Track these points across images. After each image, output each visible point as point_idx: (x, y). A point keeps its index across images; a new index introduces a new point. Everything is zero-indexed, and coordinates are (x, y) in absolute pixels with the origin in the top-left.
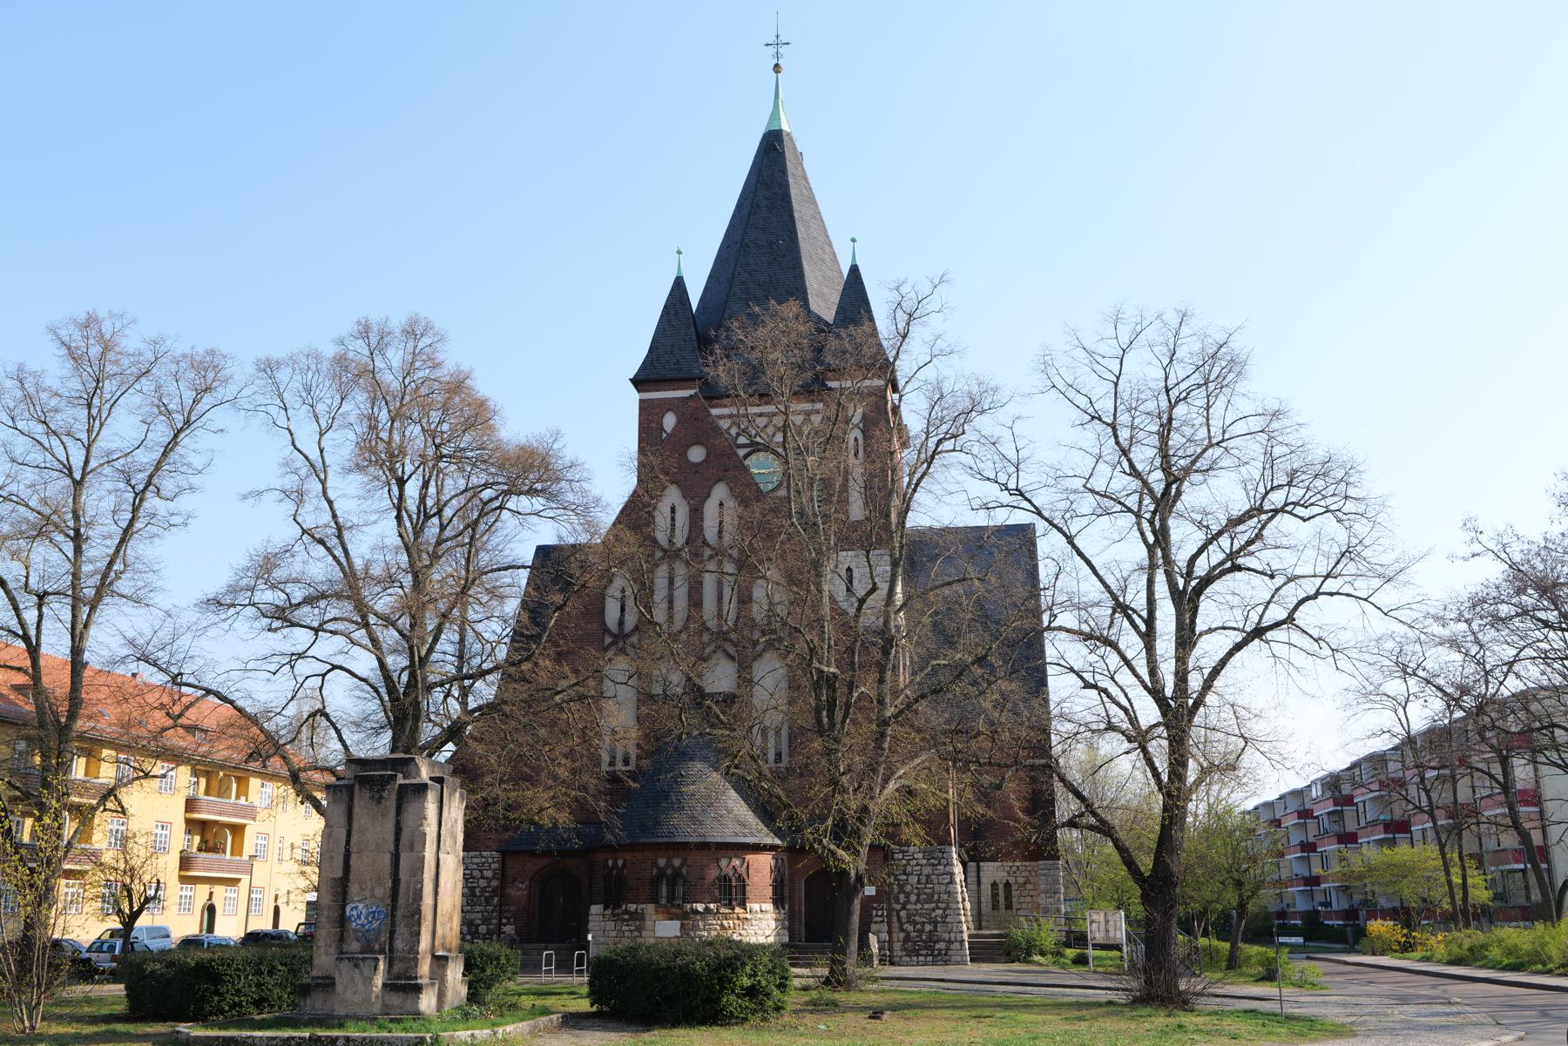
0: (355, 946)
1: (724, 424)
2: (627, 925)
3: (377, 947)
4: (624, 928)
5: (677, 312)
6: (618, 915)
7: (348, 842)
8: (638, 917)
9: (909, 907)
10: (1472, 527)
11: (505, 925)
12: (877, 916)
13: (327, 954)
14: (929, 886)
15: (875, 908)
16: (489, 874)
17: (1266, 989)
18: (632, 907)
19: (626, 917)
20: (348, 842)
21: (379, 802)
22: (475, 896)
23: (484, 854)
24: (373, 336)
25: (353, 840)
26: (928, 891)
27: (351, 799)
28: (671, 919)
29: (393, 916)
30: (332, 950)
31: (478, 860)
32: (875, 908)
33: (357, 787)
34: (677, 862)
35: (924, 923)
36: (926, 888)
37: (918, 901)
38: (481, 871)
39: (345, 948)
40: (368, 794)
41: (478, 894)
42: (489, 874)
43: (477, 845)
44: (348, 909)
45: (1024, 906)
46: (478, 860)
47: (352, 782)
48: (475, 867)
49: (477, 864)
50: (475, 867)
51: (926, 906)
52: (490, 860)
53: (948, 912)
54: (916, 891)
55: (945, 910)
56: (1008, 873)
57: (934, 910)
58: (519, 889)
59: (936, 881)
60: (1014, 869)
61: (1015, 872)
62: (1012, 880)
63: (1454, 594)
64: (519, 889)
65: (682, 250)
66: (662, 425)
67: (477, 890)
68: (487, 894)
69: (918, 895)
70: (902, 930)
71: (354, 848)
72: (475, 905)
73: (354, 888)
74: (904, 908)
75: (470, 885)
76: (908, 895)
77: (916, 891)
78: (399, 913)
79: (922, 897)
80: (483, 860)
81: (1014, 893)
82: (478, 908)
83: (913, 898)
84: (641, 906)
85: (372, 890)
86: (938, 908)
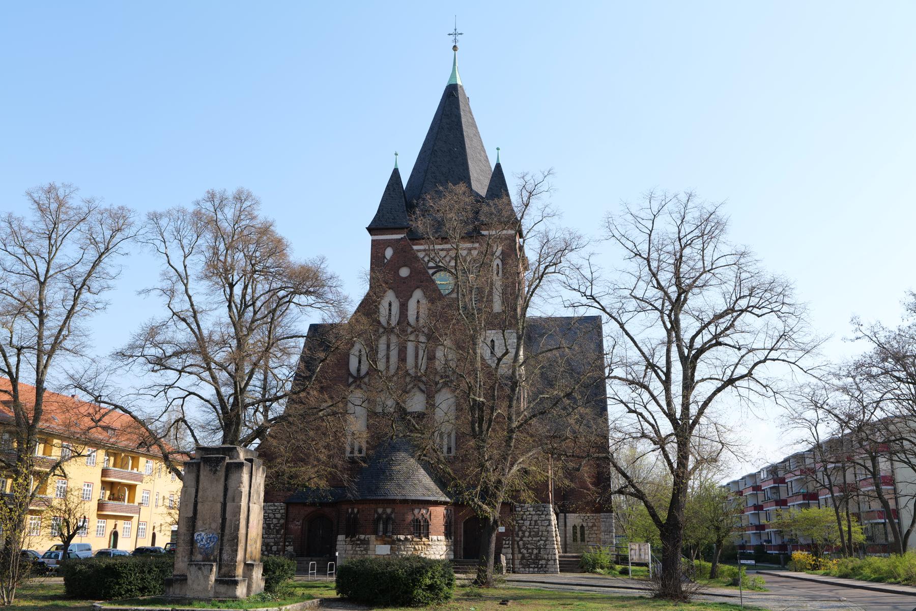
0: (199, 557)
1: (421, 255)
2: (359, 547)
3: (212, 558)
4: (357, 549)
6: (354, 541)
7: (196, 496)
8: (366, 542)
9: (524, 539)
11: (287, 546)
12: (505, 544)
15: (504, 540)
16: (278, 516)
18: (362, 537)
19: (359, 542)
20: (196, 496)
23: (276, 504)
25: (200, 494)
26: (535, 530)
27: (199, 471)
28: (385, 544)
29: (222, 540)
31: (272, 508)
32: (504, 540)
33: (202, 464)
34: (389, 511)
35: (533, 549)
36: (534, 528)
37: (530, 536)
38: (274, 514)
39: (193, 558)
41: (272, 528)
42: (278, 516)
43: (272, 499)
45: (592, 539)
46: (272, 508)
47: (199, 461)
48: (271, 511)
49: (272, 510)
50: (271, 511)
51: (534, 539)
52: (280, 508)
53: (547, 542)
54: (528, 530)
55: (545, 541)
57: (539, 541)
59: (540, 524)
60: (586, 518)
62: (585, 524)
67: (272, 525)
69: (530, 532)
71: (199, 500)
73: (199, 523)
74: (521, 540)
75: (267, 522)
76: (524, 532)
77: (528, 530)
78: (226, 538)
80: (276, 508)
82: (272, 536)
83: (527, 534)
84: (367, 536)
86: (542, 540)
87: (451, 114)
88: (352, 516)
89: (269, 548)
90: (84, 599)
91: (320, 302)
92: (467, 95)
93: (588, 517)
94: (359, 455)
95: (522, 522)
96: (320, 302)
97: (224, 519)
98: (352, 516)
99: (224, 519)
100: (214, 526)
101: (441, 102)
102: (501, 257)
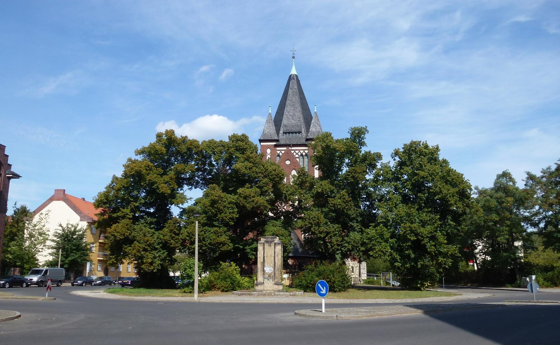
0: (267, 276)
1: (292, 152)
3: (272, 276)
5: (270, 122)
7: (264, 255)
10: (181, 136)
13: (261, 277)
20: (264, 255)
21: (270, 246)
24: (378, 153)
25: (265, 253)
27: (264, 246)
29: (275, 270)
30: (262, 277)
33: (265, 243)
39: (265, 276)
40: (268, 245)
44: (265, 268)
45: (357, 272)
47: (264, 242)
62: (354, 266)
66: (266, 151)
70: (528, 253)
71: (265, 255)
73: (266, 264)
78: (276, 269)
81: (354, 269)
85: (270, 264)
90: (74, 295)
97: (275, 263)
99: (275, 263)
100: (271, 265)
101: (287, 83)
102: (270, 154)
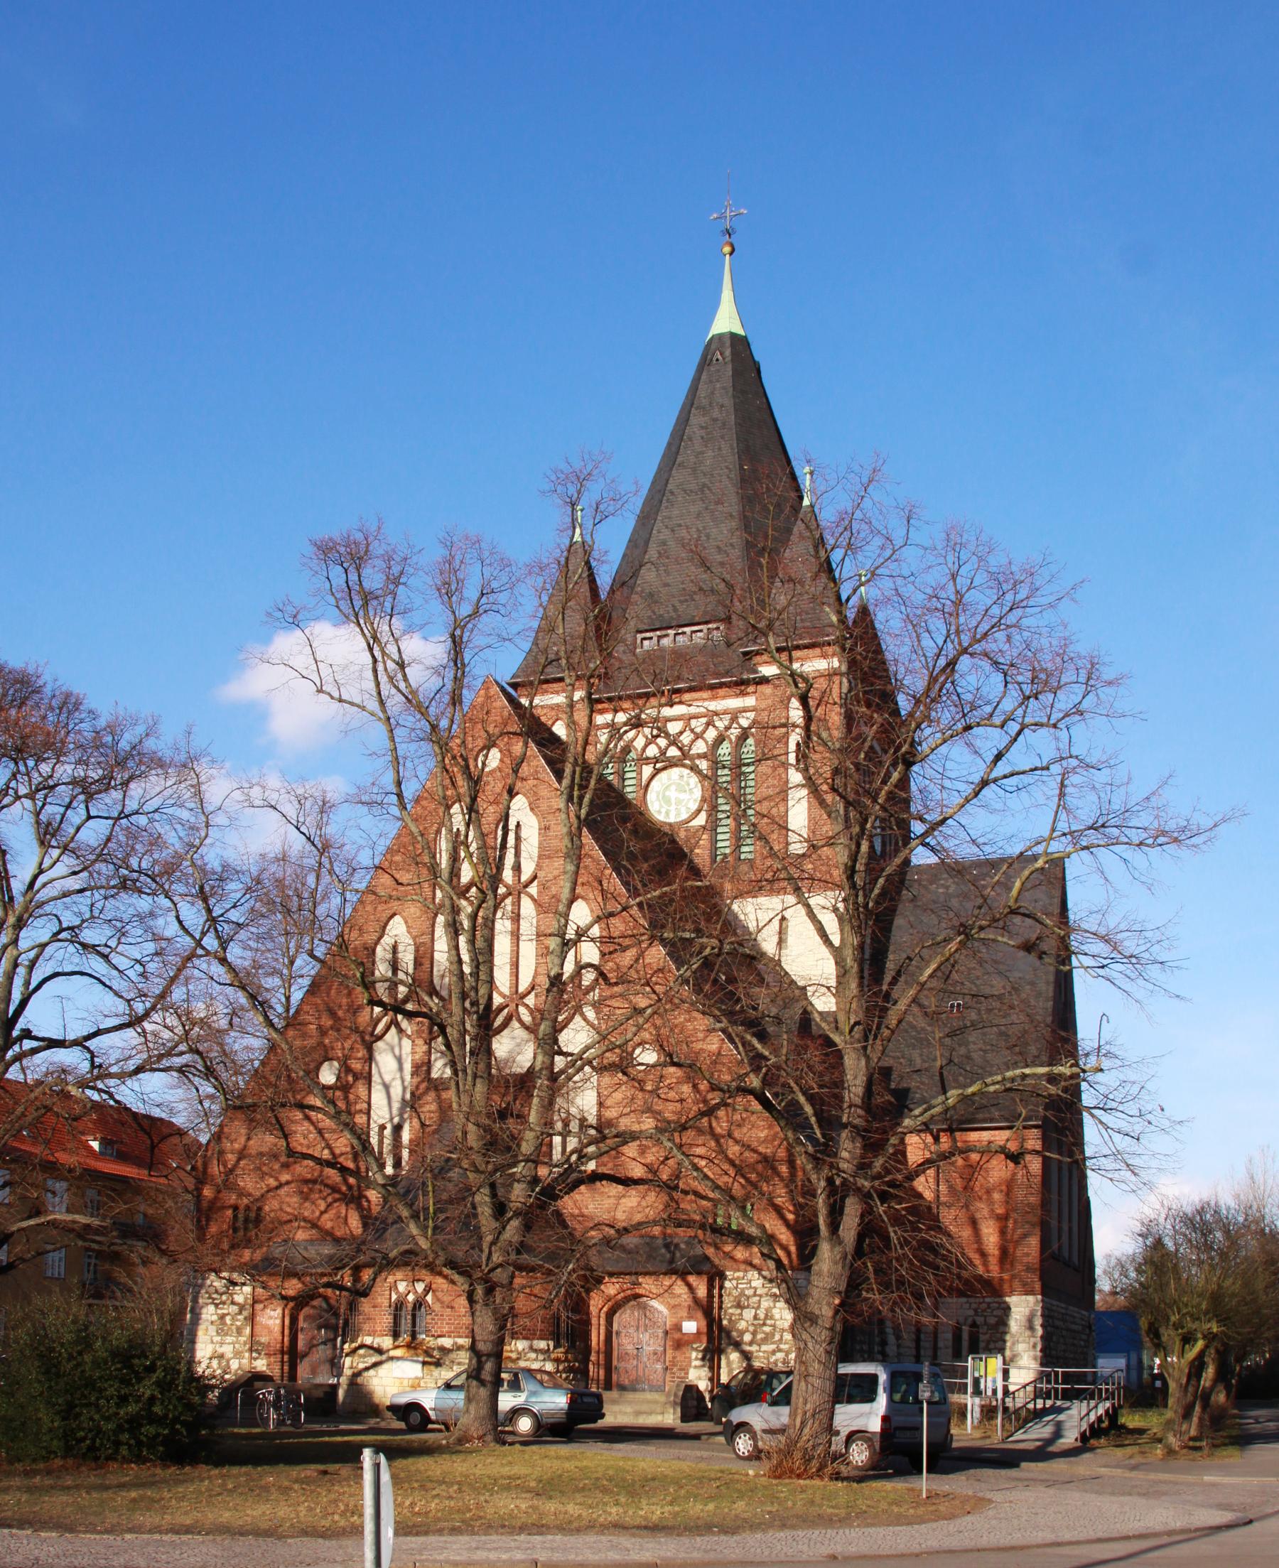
11: (256, 1359)
14: (768, 1322)
17: (1074, 1498)
22: (225, 1324)
36: (764, 1324)
54: (751, 1329)
56: (976, 1310)
57: (774, 1352)
58: (271, 1318)
60: (984, 1306)
61: (984, 1310)
62: (979, 1320)
63: (1096, 653)
64: (271, 1318)
65: (336, 527)
68: (238, 1323)
69: (754, 1334)
72: (226, 1334)
79: (759, 1336)
81: (982, 1337)
82: (229, 1339)
86: (780, 1350)
87: (711, 404)
88: (282, 1392)
89: (224, 1363)
91: (401, 1069)
92: (757, 358)
93: (989, 1304)
94: (882, 1400)
95: (739, 1311)
96: (401, 1069)
98: (282, 1392)
101: (664, 456)
